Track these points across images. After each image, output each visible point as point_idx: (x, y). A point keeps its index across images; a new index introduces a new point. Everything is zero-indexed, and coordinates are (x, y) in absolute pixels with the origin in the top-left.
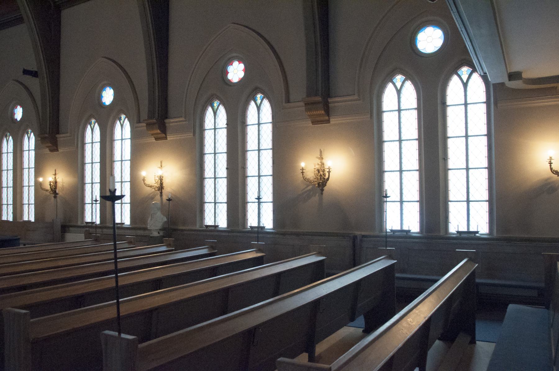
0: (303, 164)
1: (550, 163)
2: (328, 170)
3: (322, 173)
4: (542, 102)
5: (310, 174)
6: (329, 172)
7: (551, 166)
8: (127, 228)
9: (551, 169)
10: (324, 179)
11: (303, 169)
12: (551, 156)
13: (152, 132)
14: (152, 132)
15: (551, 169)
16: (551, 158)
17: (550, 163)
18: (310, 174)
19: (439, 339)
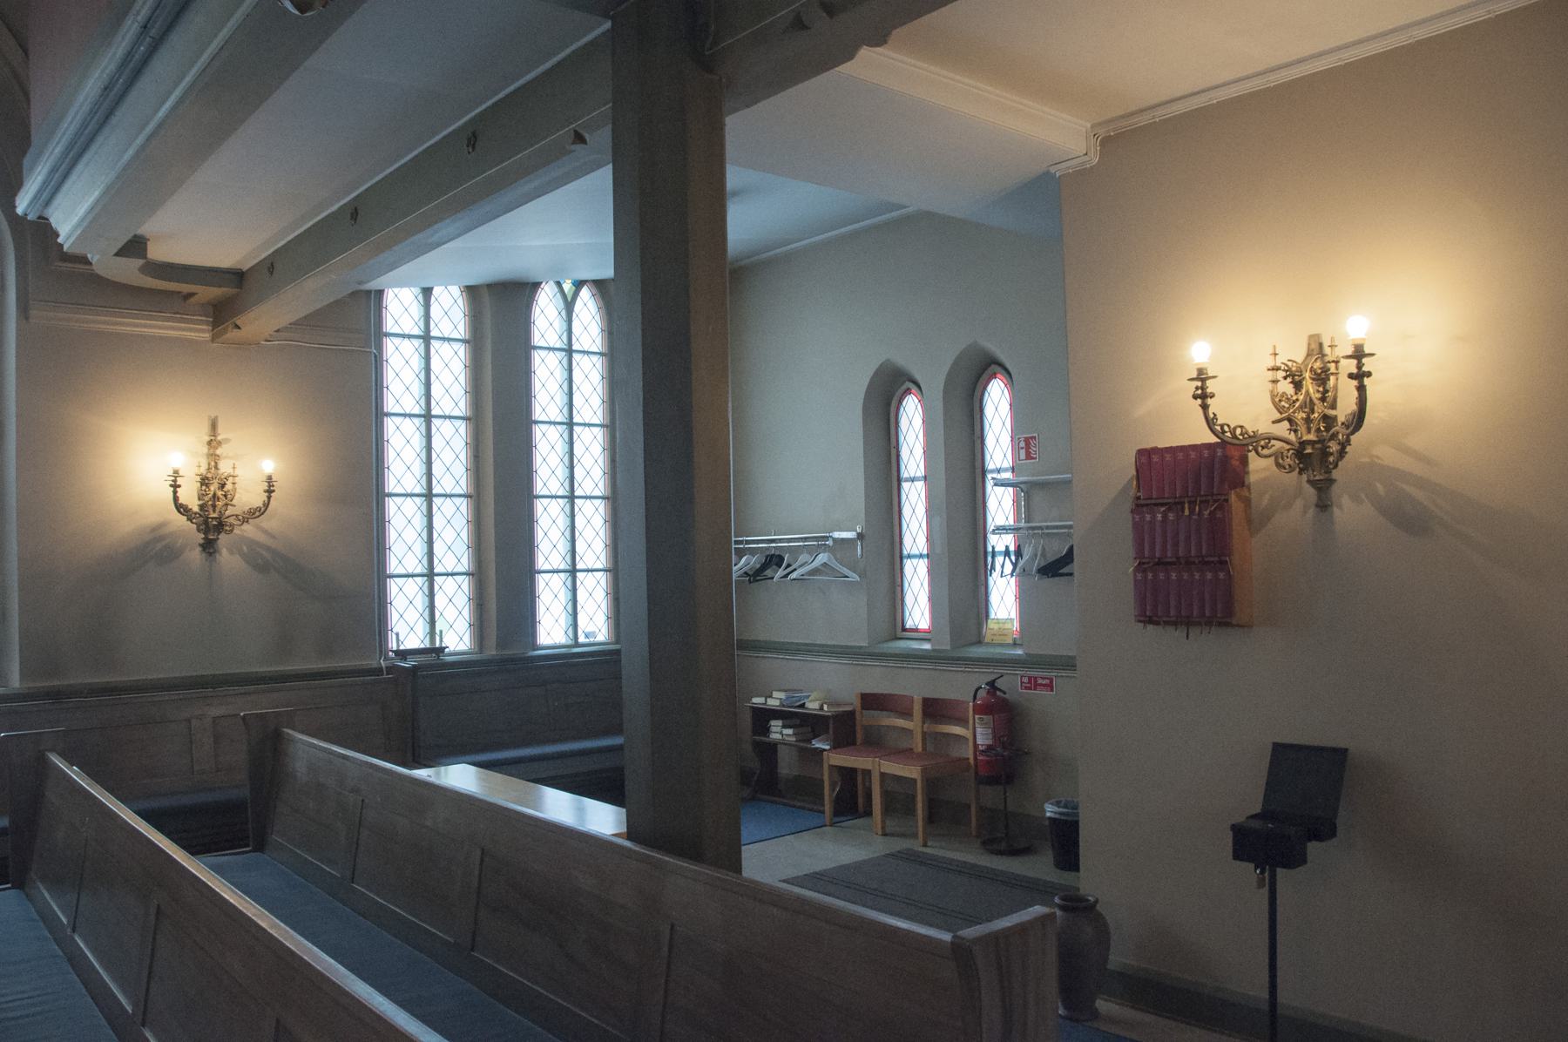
0: (1199, 352)
1: (175, 486)
2: (1350, 366)
3: (1309, 386)
4: (145, 326)
5: (1249, 404)
6: (1360, 376)
7: (175, 492)
8: (924, 631)
9: (176, 499)
10: (1329, 420)
11: (1202, 377)
12: (177, 466)
13: (903, 211)
14: (903, 211)
15: (176, 499)
16: (176, 472)
17: (175, 486)
18: (1249, 404)
19: (737, 868)
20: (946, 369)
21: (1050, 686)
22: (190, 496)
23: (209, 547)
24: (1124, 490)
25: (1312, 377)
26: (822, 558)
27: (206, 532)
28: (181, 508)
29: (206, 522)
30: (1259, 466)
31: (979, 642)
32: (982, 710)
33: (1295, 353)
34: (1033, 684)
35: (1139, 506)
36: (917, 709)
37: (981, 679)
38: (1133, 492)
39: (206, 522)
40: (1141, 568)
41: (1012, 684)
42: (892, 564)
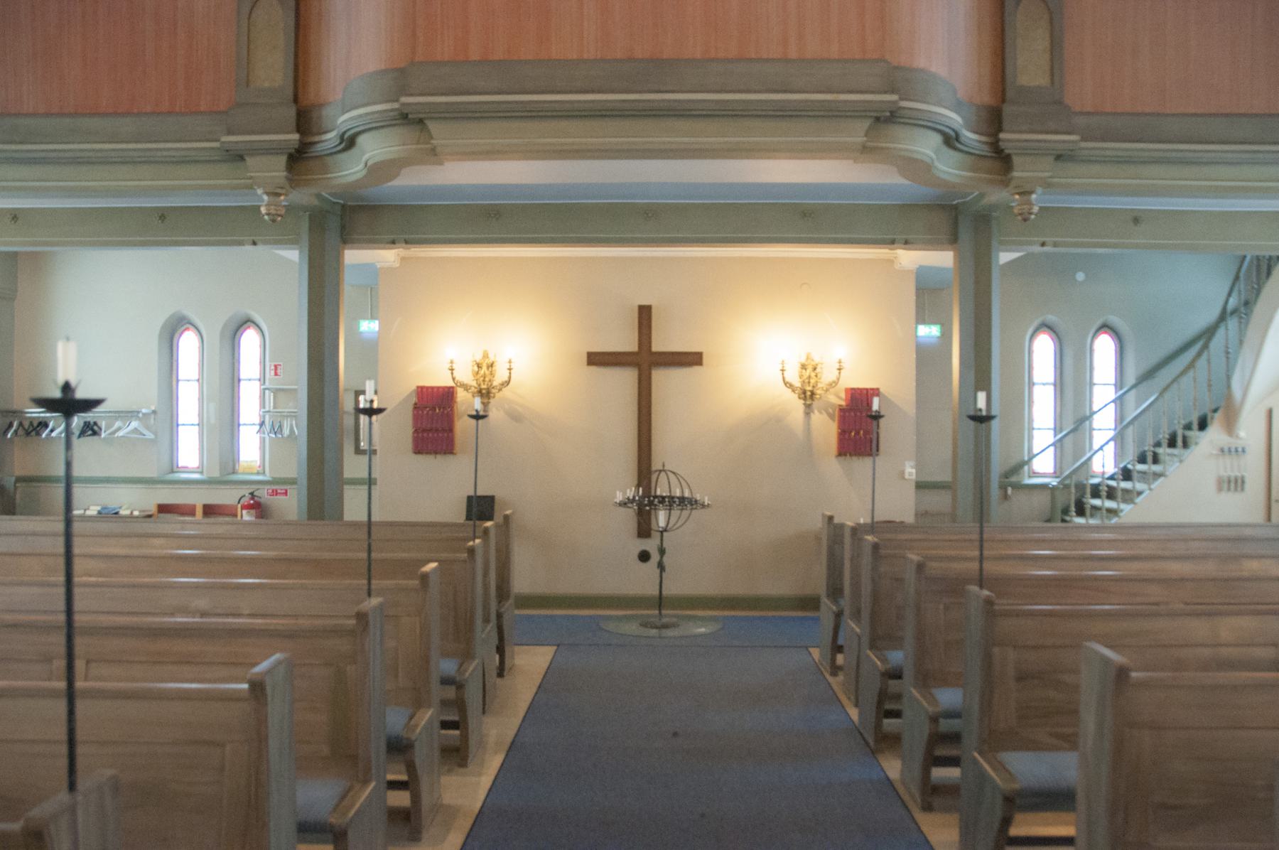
3: (484, 368)
5: (465, 375)
20: (220, 328)
21: (286, 493)
22: (794, 377)
23: (808, 409)
24: (406, 400)
25: (484, 366)
26: (134, 424)
27: (805, 399)
28: (788, 385)
29: (804, 392)
30: (461, 395)
31: (234, 472)
32: (248, 507)
33: (479, 358)
34: (275, 493)
35: (416, 407)
36: (199, 512)
37: (245, 491)
38: (414, 400)
39: (804, 392)
40: (416, 431)
41: (263, 494)
42: (172, 429)
